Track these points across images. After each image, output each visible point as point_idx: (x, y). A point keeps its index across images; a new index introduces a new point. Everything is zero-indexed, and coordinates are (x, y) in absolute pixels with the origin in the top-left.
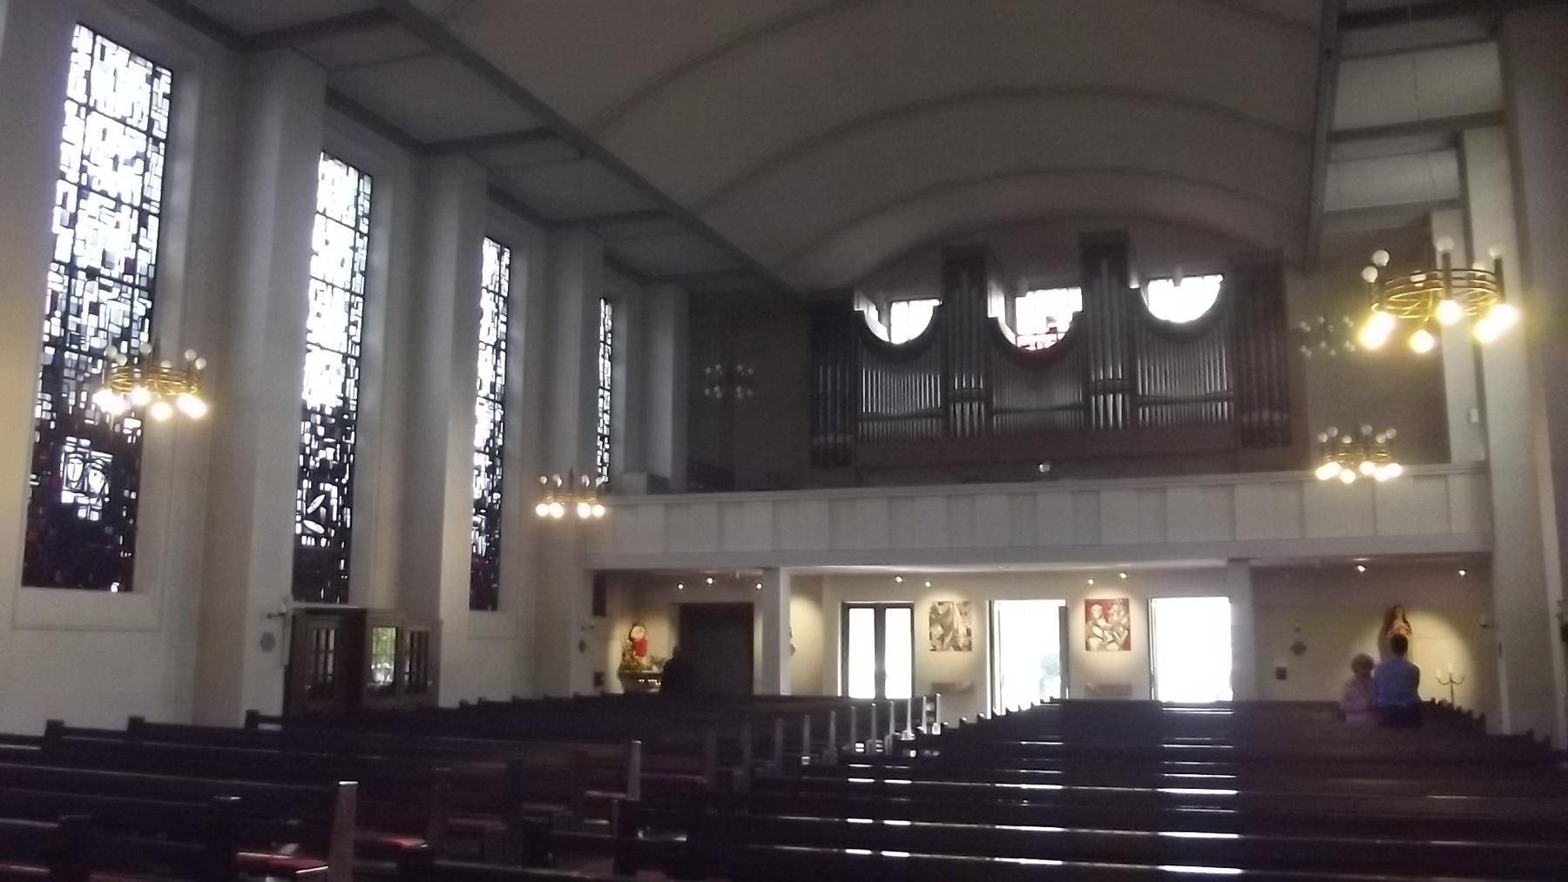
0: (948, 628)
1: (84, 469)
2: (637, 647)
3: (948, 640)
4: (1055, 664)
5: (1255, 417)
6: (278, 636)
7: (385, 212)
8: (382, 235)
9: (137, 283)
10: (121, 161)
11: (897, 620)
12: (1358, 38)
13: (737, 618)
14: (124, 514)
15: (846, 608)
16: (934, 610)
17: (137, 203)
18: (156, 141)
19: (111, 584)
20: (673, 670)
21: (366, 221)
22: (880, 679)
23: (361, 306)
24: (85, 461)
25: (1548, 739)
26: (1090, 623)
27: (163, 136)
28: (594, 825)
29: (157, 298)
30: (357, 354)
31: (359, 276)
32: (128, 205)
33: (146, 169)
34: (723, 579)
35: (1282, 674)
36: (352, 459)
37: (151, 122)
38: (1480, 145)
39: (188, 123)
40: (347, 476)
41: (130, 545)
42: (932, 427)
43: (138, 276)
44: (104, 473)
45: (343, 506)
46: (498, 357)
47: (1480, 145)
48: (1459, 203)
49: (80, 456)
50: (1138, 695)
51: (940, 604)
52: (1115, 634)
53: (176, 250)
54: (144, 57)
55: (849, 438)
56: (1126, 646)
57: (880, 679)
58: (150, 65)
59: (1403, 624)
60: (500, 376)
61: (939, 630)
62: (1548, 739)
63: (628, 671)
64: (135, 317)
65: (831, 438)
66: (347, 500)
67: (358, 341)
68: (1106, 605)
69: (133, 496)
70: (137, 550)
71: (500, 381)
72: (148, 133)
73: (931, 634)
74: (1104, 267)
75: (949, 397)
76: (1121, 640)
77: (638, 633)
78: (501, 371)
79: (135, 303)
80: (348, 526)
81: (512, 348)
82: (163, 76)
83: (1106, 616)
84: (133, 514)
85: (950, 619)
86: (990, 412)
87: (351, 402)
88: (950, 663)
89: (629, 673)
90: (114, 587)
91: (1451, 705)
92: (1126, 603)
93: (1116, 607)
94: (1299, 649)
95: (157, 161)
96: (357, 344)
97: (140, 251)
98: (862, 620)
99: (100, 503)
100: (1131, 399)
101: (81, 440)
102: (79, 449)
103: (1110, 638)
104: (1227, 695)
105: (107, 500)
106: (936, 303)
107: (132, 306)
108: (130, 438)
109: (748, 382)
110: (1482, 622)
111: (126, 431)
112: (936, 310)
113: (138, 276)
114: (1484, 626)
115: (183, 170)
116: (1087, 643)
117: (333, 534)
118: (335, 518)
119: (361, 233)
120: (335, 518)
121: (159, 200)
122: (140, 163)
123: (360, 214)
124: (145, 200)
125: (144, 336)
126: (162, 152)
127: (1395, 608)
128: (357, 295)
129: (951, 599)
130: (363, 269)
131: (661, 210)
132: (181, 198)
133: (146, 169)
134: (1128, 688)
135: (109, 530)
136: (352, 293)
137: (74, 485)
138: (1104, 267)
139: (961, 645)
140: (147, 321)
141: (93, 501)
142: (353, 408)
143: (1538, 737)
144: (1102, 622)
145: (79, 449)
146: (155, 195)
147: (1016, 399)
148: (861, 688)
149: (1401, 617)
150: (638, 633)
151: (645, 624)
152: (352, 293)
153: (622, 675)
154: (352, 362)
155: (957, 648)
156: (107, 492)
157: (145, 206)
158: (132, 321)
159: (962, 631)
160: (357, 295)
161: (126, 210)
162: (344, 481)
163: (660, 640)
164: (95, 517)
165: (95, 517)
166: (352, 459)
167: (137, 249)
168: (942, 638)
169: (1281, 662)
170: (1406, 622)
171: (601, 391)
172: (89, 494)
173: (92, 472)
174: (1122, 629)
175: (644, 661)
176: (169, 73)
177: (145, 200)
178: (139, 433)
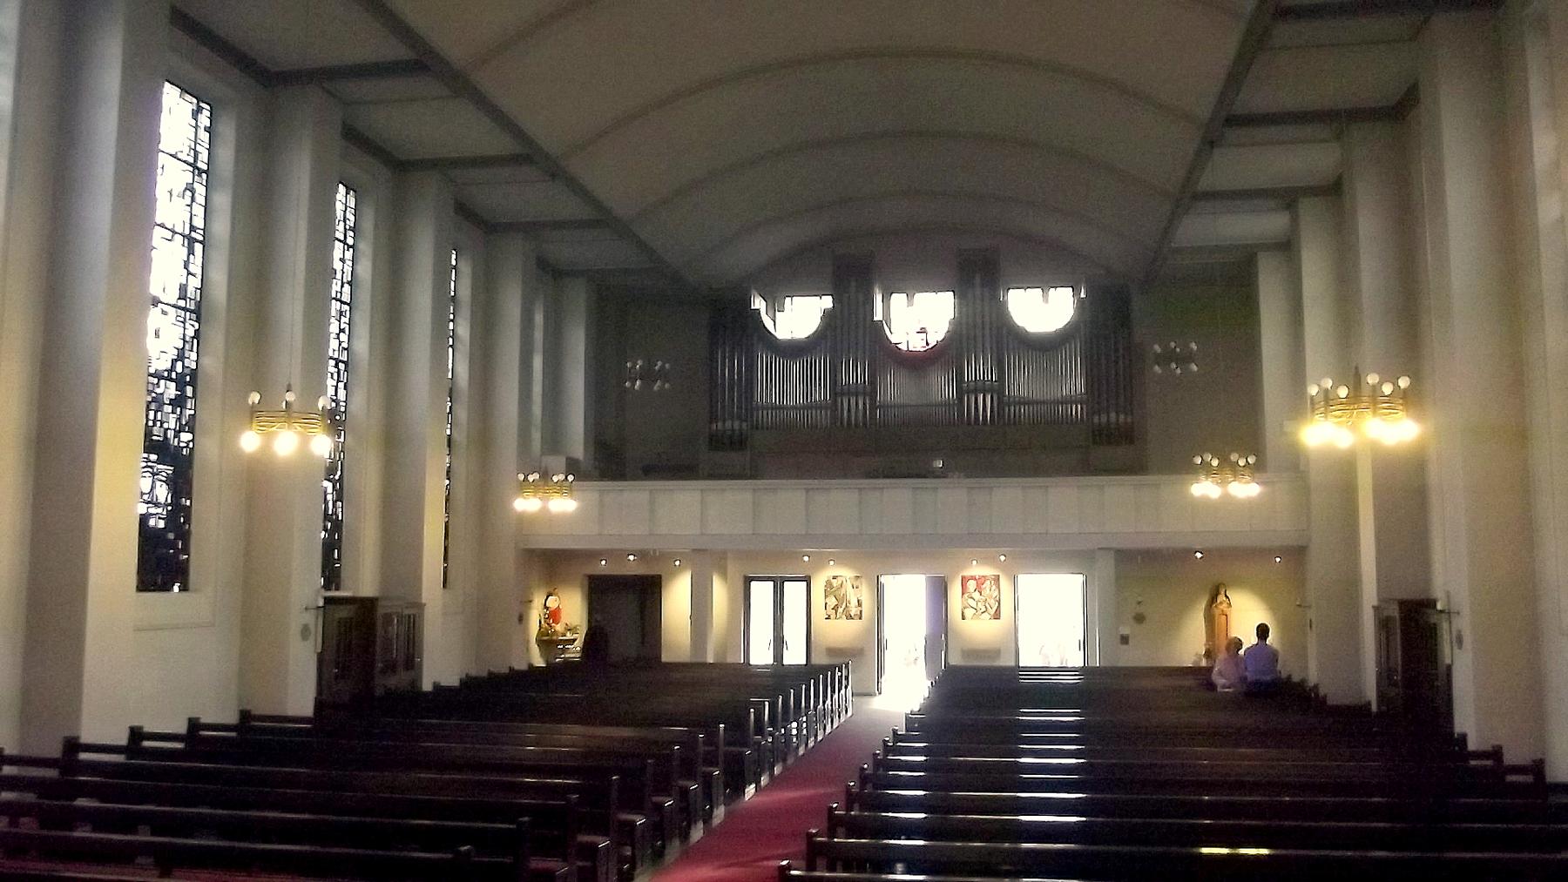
0: (841, 600)
1: (153, 482)
2: (553, 615)
3: (840, 610)
4: (1049, 663)
5: (1104, 419)
6: (312, 628)
7: (368, 225)
8: (365, 247)
9: (188, 306)
10: (174, 193)
11: (794, 592)
12: (1233, 134)
13: (648, 590)
14: (182, 521)
15: (748, 581)
16: (829, 584)
17: (187, 232)
18: (201, 172)
19: (174, 585)
20: (596, 638)
21: (352, 234)
22: (779, 642)
23: (348, 313)
24: (154, 474)
25: (1289, 677)
26: (966, 595)
27: (205, 168)
28: (514, 783)
29: (202, 321)
30: (346, 360)
31: (346, 286)
32: (177, 233)
33: (193, 200)
34: (642, 555)
35: (1125, 640)
36: (342, 457)
37: (196, 154)
38: (1309, 210)
39: (226, 155)
40: (339, 473)
41: (186, 550)
42: (823, 418)
43: (188, 300)
44: (167, 484)
45: (336, 501)
46: (191, 252)
47: (1309, 210)
48: (1287, 247)
49: (151, 470)
50: (1006, 661)
51: (834, 578)
52: (987, 605)
53: (219, 278)
54: (191, 95)
55: (744, 425)
56: (997, 616)
57: (779, 642)
58: (195, 101)
59: (1224, 598)
60: (194, 275)
61: (832, 602)
62: (1289, 677)
63: (546, 638)
64: (187, 339)
65: (728, 424)
66: (339, 496)
67: (346, 346)
68: (980, 581)
69: (188, 503)
70: (192, 554)
71: (195, 283)
72: (194, 165)
73: (826, 604)
74: (978, 280)
75: (837, 391)
76: (992, 612)
77: (553, 602)
78: (196, 268)
79: (187, 325)
80: (340, 518)
81: (458, 345)
82: (204, 111)
83: (979, 589)
84: (188, 520)
85: (843, 591)
86: (874, 407)
87: (341, 404)
88: (838, 632)
89: (548, 642)
90: (176, 588)
91: (1302, 683)
92: (997, 579)
93: (988, 582)
94: (1140, 619)
95: (200, 190)
96: (345, 349)
97: (190, 276)
98: (762, 593)
99: (165, 513)
100: (999, 398)
101: (151, 455)
102: (149, 464)
103: (984, 609)
104: (1076, 660)
105: (170, 508)
106: (827, 302)
107: (185, 329)
108: (185, 449)
109: (663, 375)
110: (1298, 603)
111: (182, 445)
112: (828, 316)
113: (188, 300)
114: (1299, 606)
115: (223, 200)
116: (963, 613)
117: (329, 527)
118: (330, 512)
119: (348, 245)
120: (330, 512)
121: (202, 227)
122: (188, 194)
123: (348, 227)
124: (193, 228)
125: (194, 356)
126: (204, 183)
127: (1220, 584)
128: (345, 303)
129: (846, 573)
130: (350, 279)
131: (602, 220)
132: (222, 227)
133: (193, 200)
134: (997, 653)
135: (171, 536)
136: (342, 302)
137: (146, 497)
138: (978, 280)
139: (852, 615)
140: (195, 341)
141: (160, 510)
142: (343, 409)
143: (1296, 678)
144: (976, 595)
145: (149, 464)
146: (199, 222)
147: (895, 390)
148: (761, 655)
149: (1223, 592)
150: (553, 602)
151: (559, 594)
152: (342, 302)
153: (540, 642)
154: (342, 366)
155: (850, 617)
156: (169, 501)
157: (193, 234)
158: (185, 341)
159: (854, 602)
160: (345, 303)
161: (179, 238)
162: (337, 477)
163: (572, 609)
164: (161, 524)
165: (161, 524)
166: (342, 457)
167: (188, 274)
168: (835, 608)
169: (1125, 631)
170: (1227, 597)
171: (335, 305)
172: (157, 505)
173: (158, 483)
174: (993, 601)
175: (559, 628)
176: (209, 108)
177: (193, 228)
178: (191, 445)
